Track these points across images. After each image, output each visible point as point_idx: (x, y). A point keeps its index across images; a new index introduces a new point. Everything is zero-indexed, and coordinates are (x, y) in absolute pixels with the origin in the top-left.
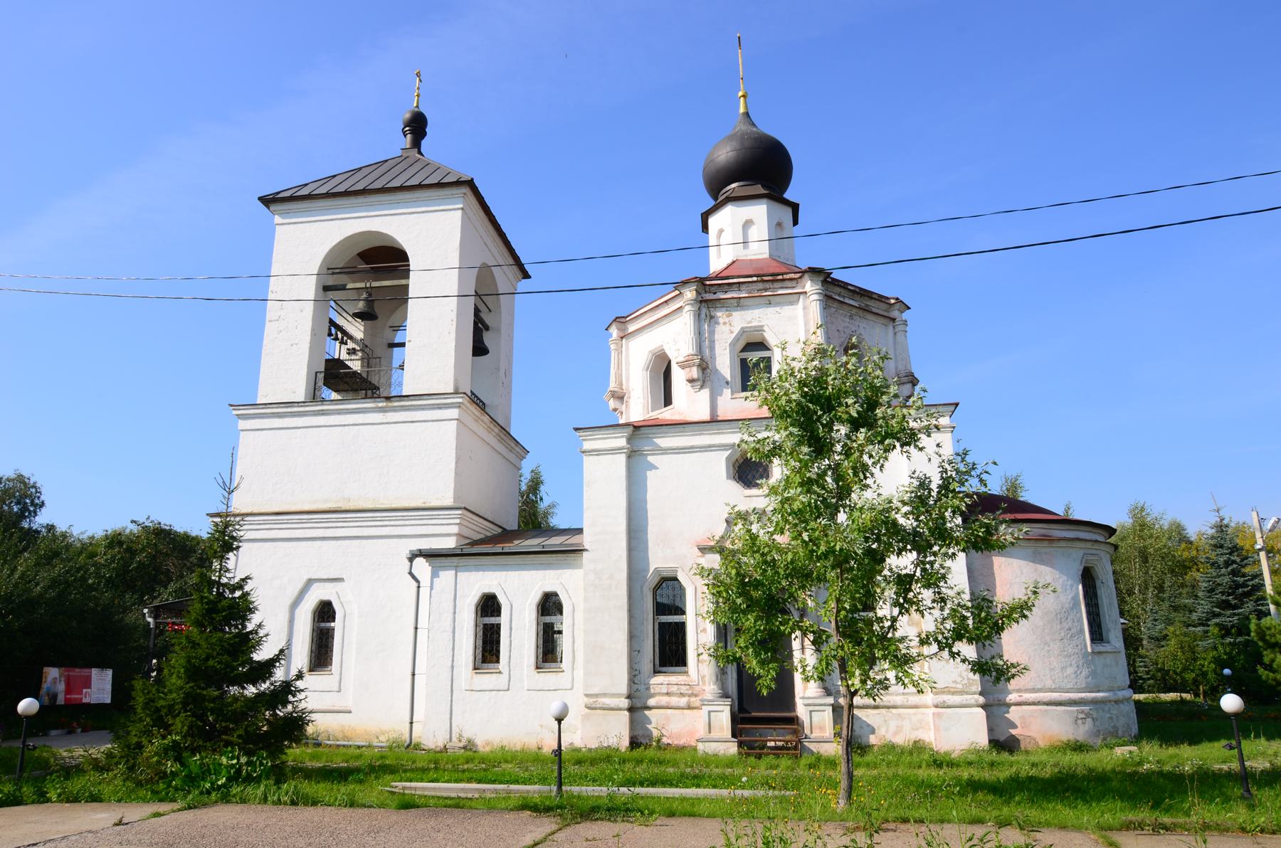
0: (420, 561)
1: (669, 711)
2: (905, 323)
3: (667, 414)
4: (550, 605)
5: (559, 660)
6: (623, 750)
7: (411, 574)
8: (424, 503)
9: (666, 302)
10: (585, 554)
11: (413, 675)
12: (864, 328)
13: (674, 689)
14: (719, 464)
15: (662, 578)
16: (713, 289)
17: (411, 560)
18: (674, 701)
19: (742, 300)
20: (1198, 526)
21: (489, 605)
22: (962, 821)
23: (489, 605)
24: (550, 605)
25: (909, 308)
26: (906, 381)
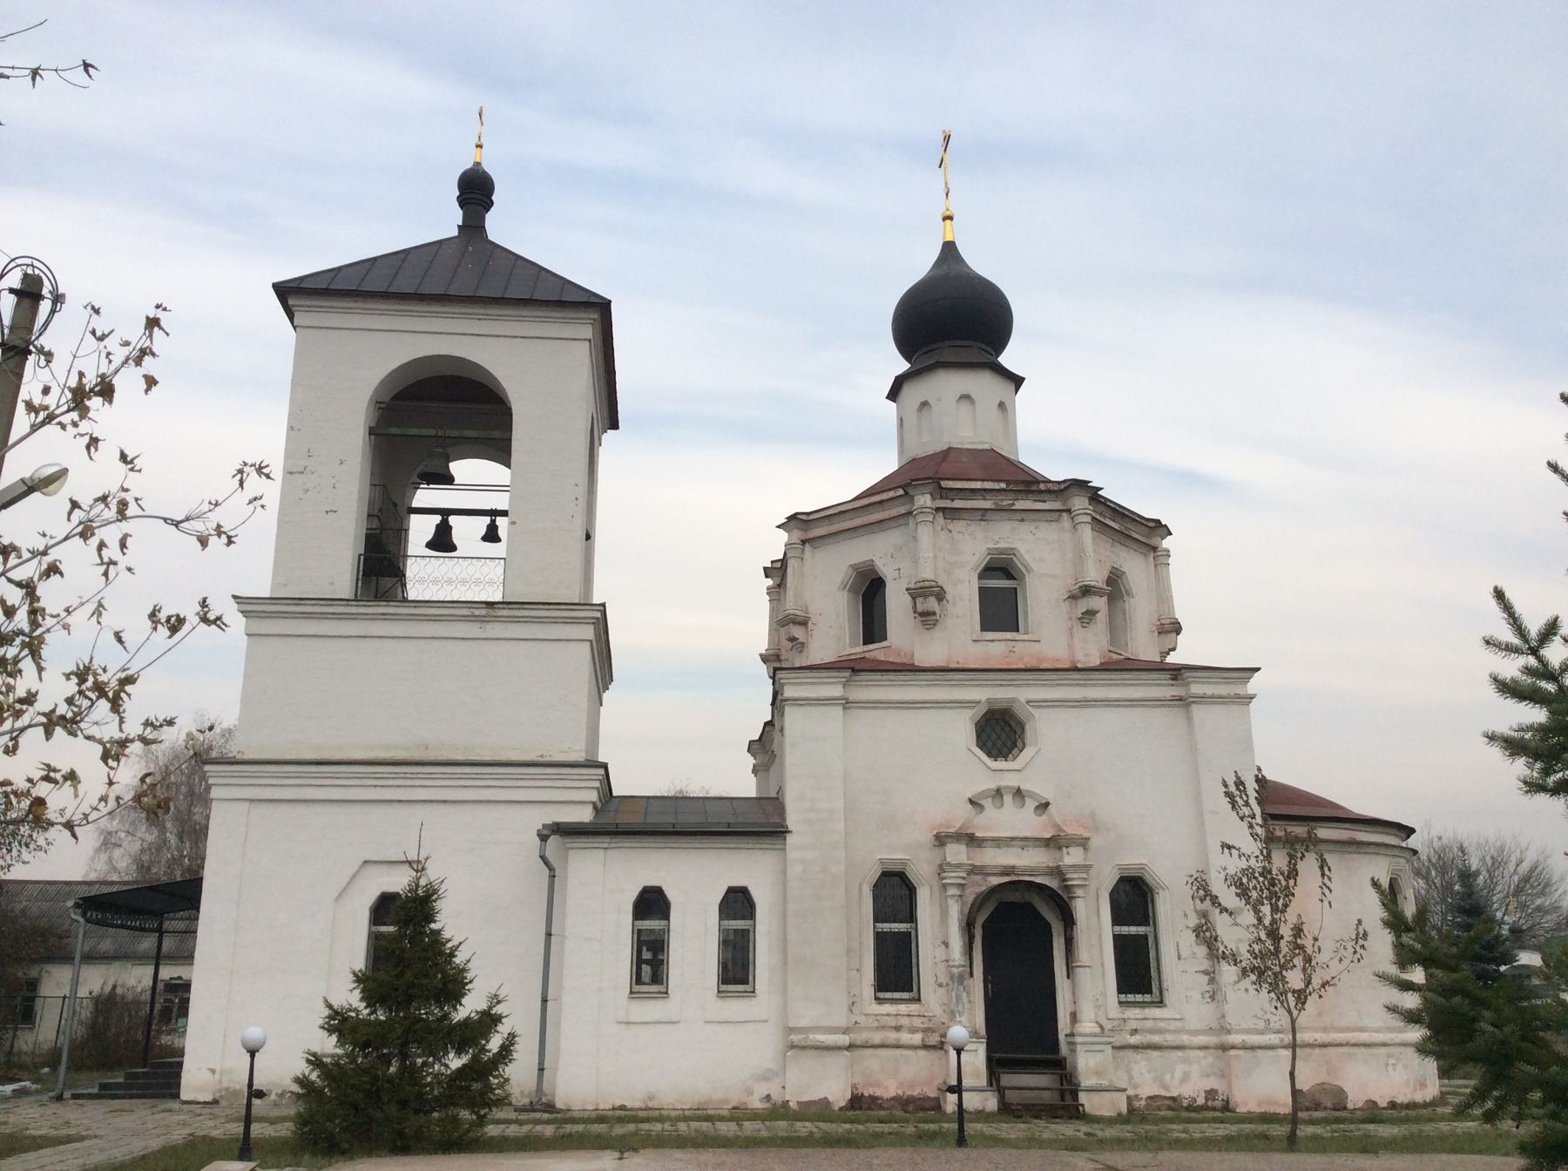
0: (553, 840)
1: (898, 1052)
2: (1167, 554)
3: (876, 651)
4: (737, 903)
5: (881, 995)
6: (339, 1051)
7: (543, 858)
8: (542, 756)
9: (881, 502)
10: (788, 836)
11: (544, 1001)
12: (1125, 558)
13: (905, 1021)
14: (961, 728)
15: (903, 873)
16: (951, 494)
17: (543, 838)
18: (905, 1037)
19: (989, 513)
20: (768, 598)
21: (652, 903)
22: (149, 1108)
23: (652, 903)
24: (737, 903)
25: (1171, 534)
26: (1170, 629)
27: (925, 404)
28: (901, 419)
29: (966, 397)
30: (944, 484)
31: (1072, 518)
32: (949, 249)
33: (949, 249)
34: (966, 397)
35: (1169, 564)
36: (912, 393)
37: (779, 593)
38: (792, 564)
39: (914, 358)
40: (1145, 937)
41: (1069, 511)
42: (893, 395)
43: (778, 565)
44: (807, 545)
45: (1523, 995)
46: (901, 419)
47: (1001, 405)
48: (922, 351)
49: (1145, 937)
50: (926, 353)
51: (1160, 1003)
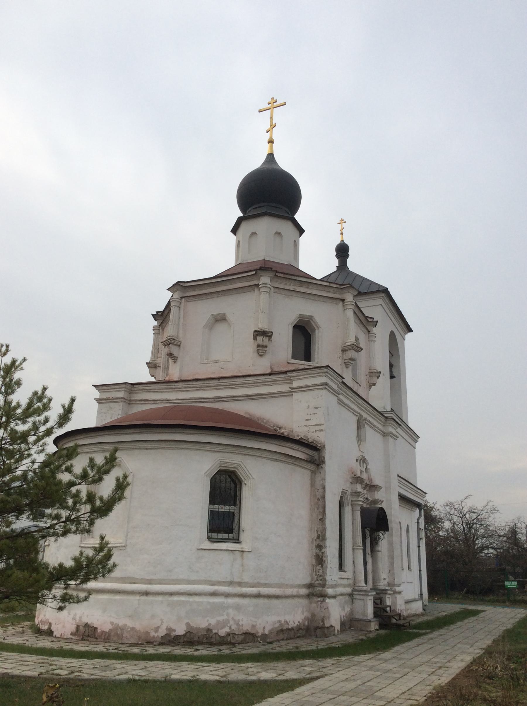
20: (153, 332)
27: (254, 234)
28: (239, 241)
29: (278, 234)
30: (277, 274)
31: (344, 306)
32: (271, 157)
33: (271, 157)
34: (278, 234)
35: (375, 341)
36: (246, 228)
37: (159, 330)
38: (174, 311)
39: (250, 209)
40: (233, 514)
41: (343, 300)
42: (234, 231)
43: (160, 314)
44: (183, 299)
45: (23, 451)
46: (239, 241)
47: (295, 241)
48: (254, 207)
49: (233, 514)
50: (255, 208)
51: (237, 540)
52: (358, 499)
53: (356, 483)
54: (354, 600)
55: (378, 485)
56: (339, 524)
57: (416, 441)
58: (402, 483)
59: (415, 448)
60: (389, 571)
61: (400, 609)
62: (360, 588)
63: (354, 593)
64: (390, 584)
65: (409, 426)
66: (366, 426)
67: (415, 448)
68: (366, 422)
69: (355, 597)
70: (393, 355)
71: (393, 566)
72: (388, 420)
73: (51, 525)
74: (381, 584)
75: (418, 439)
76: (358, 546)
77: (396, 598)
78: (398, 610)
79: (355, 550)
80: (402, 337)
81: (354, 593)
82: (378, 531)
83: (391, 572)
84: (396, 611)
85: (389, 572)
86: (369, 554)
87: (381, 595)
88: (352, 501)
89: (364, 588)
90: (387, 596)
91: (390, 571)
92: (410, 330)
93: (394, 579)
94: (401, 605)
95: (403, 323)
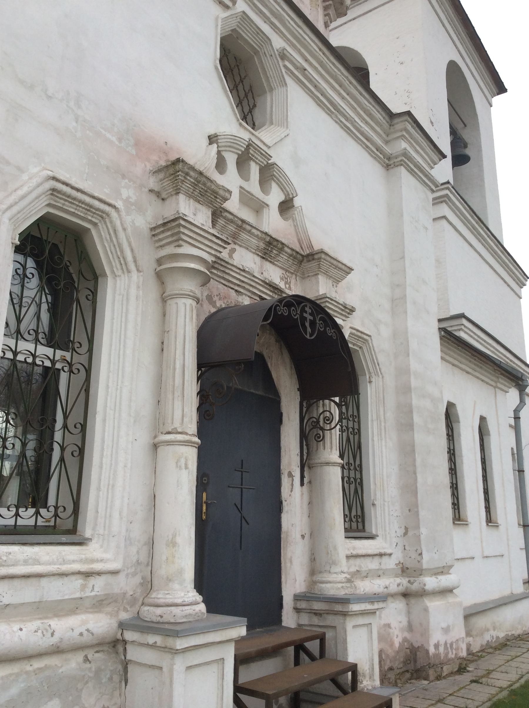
52: (181, 251)
53: (177, 194)
54: (130, 668)
55: (322, 252)
56: (483, 476)
57: (522, 285)
58: (476, 337)
59: (521, 298)
60: (403, 531)
61: (442, 642)
62: (159, 611)
63: (129, 636)
64: (407, 568)
65: (505, 246)
66: (289, 81)
67: (521, 298)
68: (287, 63)
69: (133, 653)
70: (465, 126)
71: (417, 513)
72: (396, 121)
73: (17, 474)
74: (332, 577)
75: (527, 281)
76: (169, 433)
77: (426, 610)
78: (437, 646)
79: (162, 450)
80: (487, 100)
81: (129, 636)
82: (323, 399)
83: (410, 533)
84: (427, 652)
85: (405, 534)
86: (290, 475)
87: (330, 620)
88: (159, 262)
89: (188, 610)
90: (350, 623)
91: (406, 529)
92: (501, 89)
93: (421, 554)
94: (446, 630)
95: (483, 64)
